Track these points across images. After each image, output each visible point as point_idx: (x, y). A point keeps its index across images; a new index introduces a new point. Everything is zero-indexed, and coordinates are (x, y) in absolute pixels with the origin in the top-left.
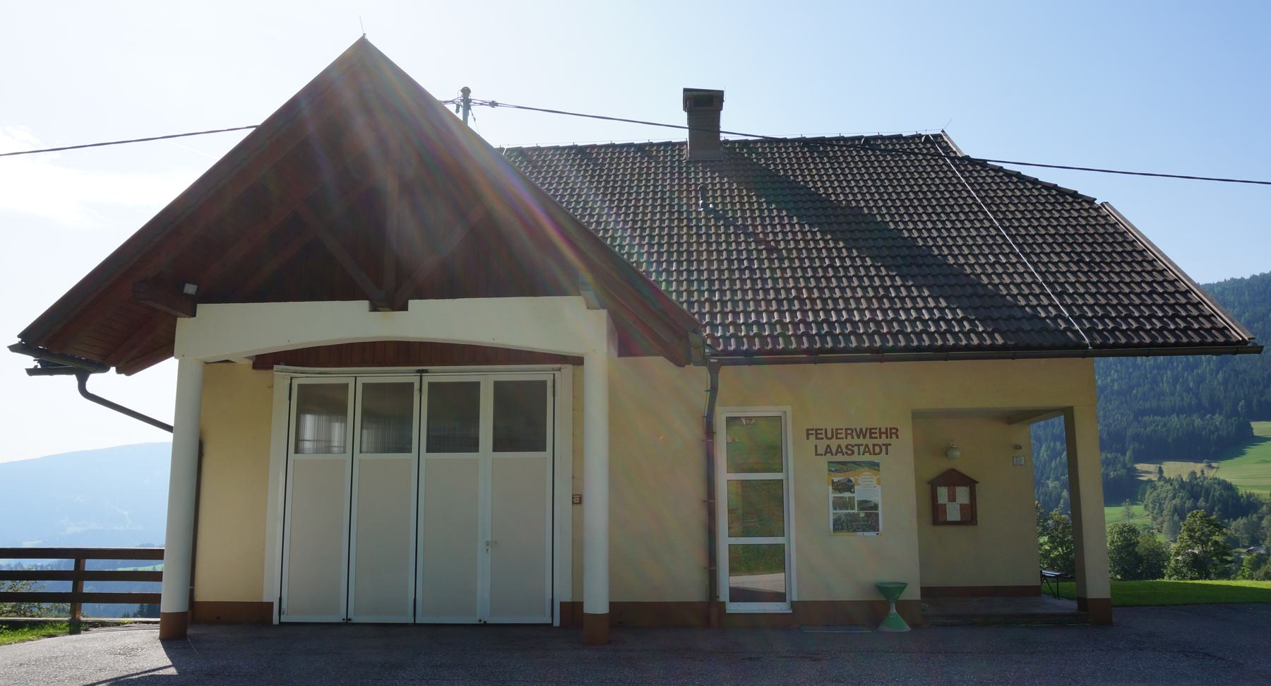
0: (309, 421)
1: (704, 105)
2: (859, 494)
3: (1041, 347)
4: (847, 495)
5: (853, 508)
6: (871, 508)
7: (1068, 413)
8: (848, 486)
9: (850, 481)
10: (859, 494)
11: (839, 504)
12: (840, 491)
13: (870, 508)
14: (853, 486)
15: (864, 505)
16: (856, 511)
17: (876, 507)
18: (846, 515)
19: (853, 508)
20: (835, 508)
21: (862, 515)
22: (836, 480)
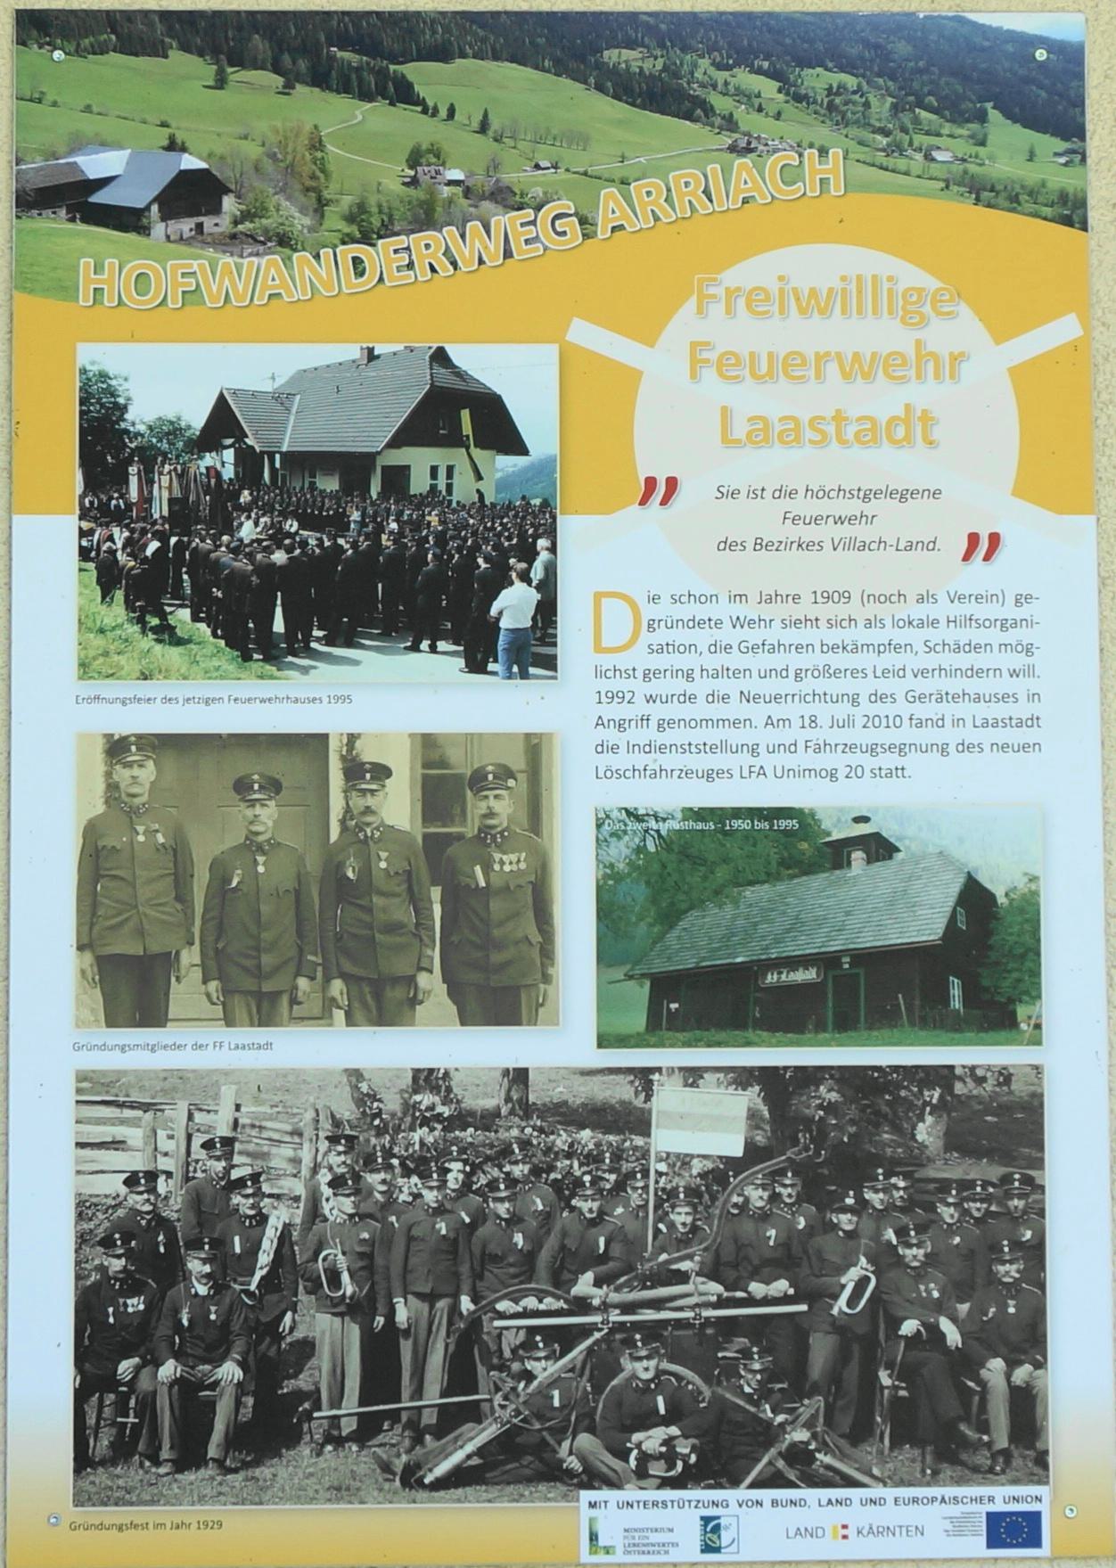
0: (491, 667)
1: (221, 82)
2: (629, 710)
3: (95, 905)
4: (387, 699)
5: (499, 987)
6: (877, 985)
7: (598, 597)
8: (391, 540)
9: (461, 412)
10: (629, 710)
11: (178, 914)
12: (266, 616)
13: (863, 993)
14: (525, 530)
15: (725, 920)
16: (566, 1038)
17: (982, 958)
18: (364, 1132)
19: (499, 987)
20: (130, 986)
21: (701, 1117)
22: (167, 387)
